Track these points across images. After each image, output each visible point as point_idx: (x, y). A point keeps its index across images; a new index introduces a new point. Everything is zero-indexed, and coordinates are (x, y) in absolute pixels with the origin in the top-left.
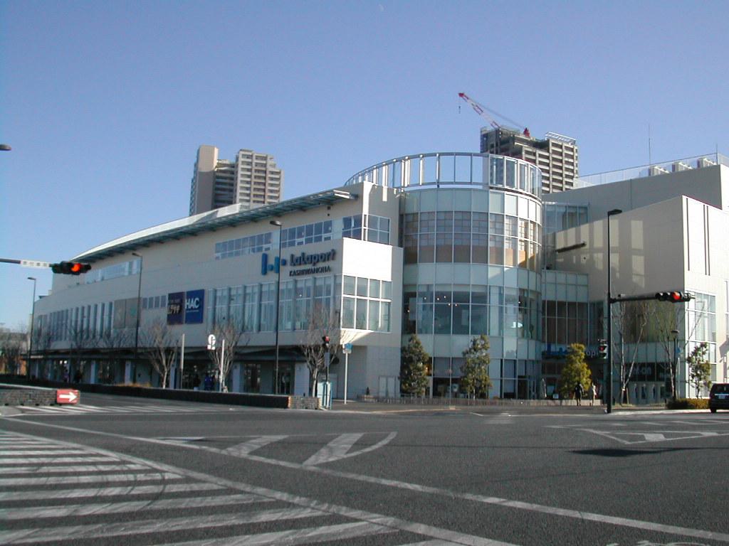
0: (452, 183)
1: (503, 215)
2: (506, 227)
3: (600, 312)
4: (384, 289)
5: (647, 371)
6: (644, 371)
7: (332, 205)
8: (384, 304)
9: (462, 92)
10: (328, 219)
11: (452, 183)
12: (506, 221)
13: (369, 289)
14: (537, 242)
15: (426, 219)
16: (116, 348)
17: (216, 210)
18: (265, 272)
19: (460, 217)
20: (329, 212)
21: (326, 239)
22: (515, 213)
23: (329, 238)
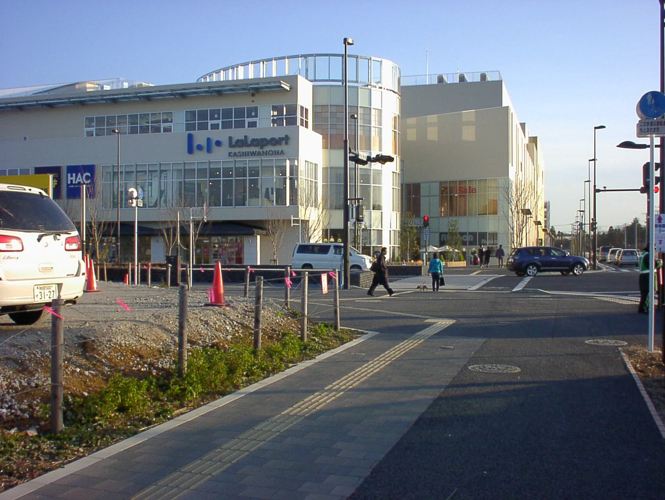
0: (327, 81)
1: (358, 107)
2: (373, 118)
3: (497, 203)
4: (650, 329)
5: (468, 238)
6: (465, 238)
7: (258, 92)
8: (152, 117)
9: (37, 241)
10: (253, 105)
11: (327, 81)
12: (373, 111)
13: (653, 345)
14: (397, 131)
15: (335, 111)
16: (216, 82)
17: (299, 284)
18: (190, 151)
19: (334, 110)
20: (253, 98)
21: (166, 130)
22: (380, 106)
23: (167, 130)
